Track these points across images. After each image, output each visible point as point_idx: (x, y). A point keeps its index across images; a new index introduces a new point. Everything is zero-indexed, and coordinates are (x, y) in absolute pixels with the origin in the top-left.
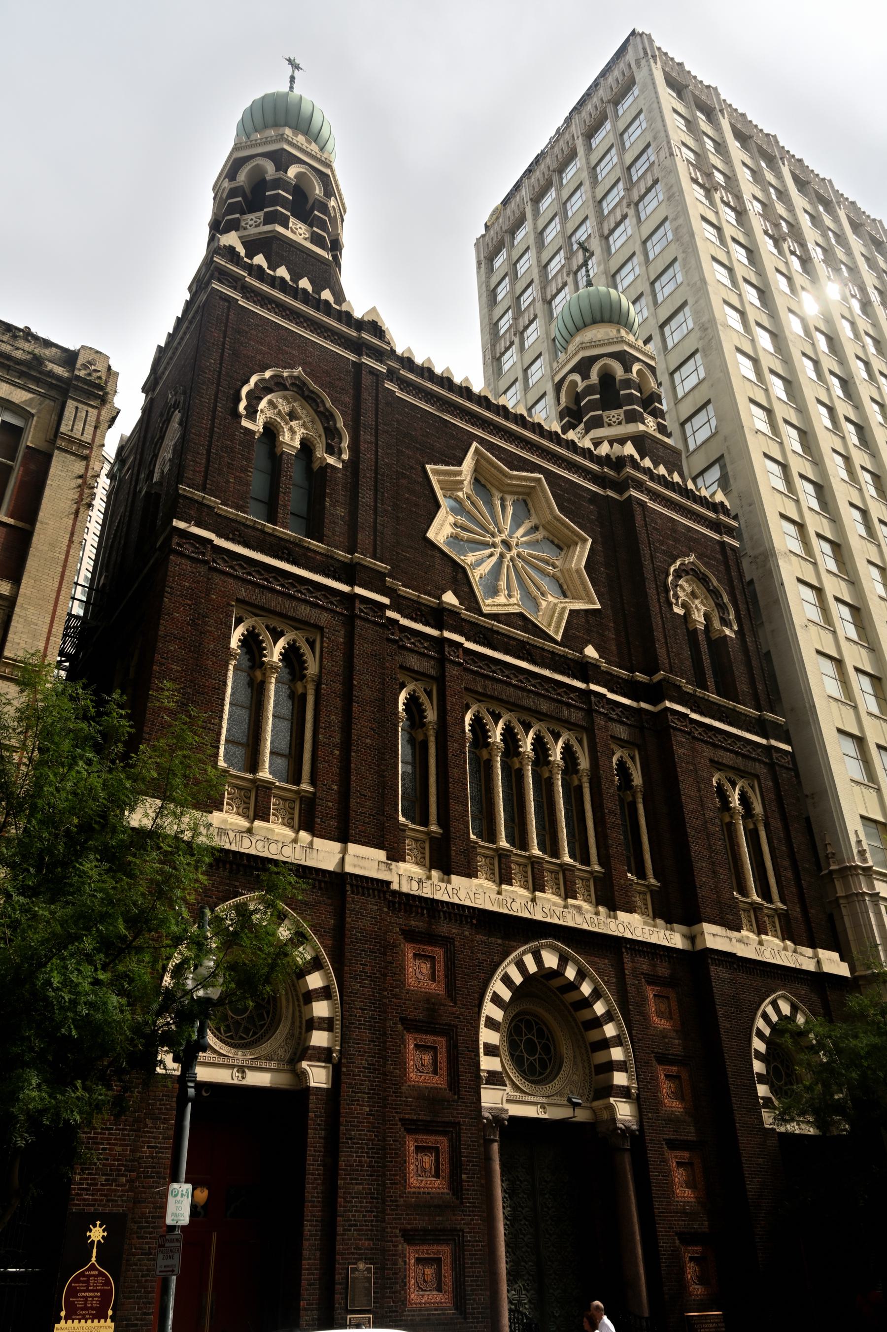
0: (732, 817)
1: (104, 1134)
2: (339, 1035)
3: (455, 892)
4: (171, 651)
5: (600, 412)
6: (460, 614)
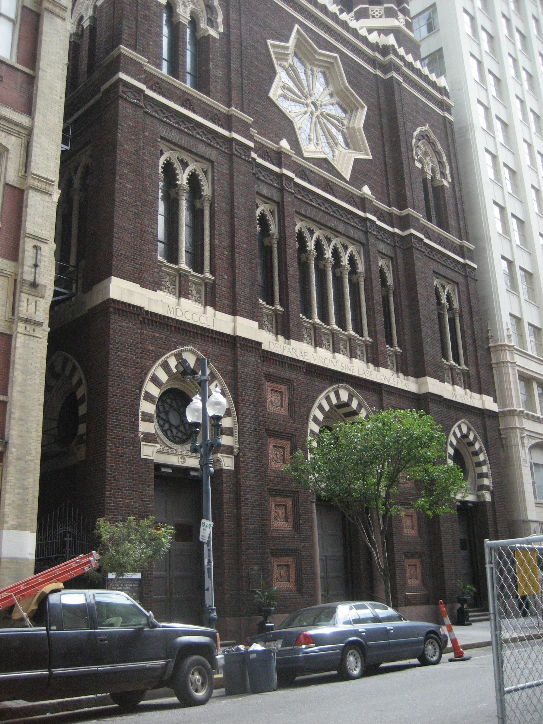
0: (202, 204)
1: (119, 492)
2: (237, 438)
3: (294, 351)
4: (125, 174)
5: (367, 6)
6: (291, 156)
